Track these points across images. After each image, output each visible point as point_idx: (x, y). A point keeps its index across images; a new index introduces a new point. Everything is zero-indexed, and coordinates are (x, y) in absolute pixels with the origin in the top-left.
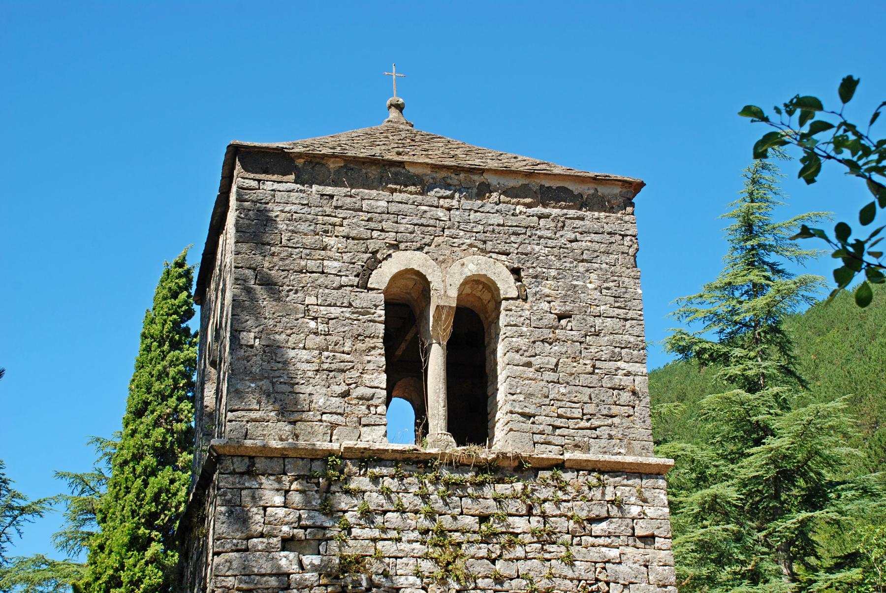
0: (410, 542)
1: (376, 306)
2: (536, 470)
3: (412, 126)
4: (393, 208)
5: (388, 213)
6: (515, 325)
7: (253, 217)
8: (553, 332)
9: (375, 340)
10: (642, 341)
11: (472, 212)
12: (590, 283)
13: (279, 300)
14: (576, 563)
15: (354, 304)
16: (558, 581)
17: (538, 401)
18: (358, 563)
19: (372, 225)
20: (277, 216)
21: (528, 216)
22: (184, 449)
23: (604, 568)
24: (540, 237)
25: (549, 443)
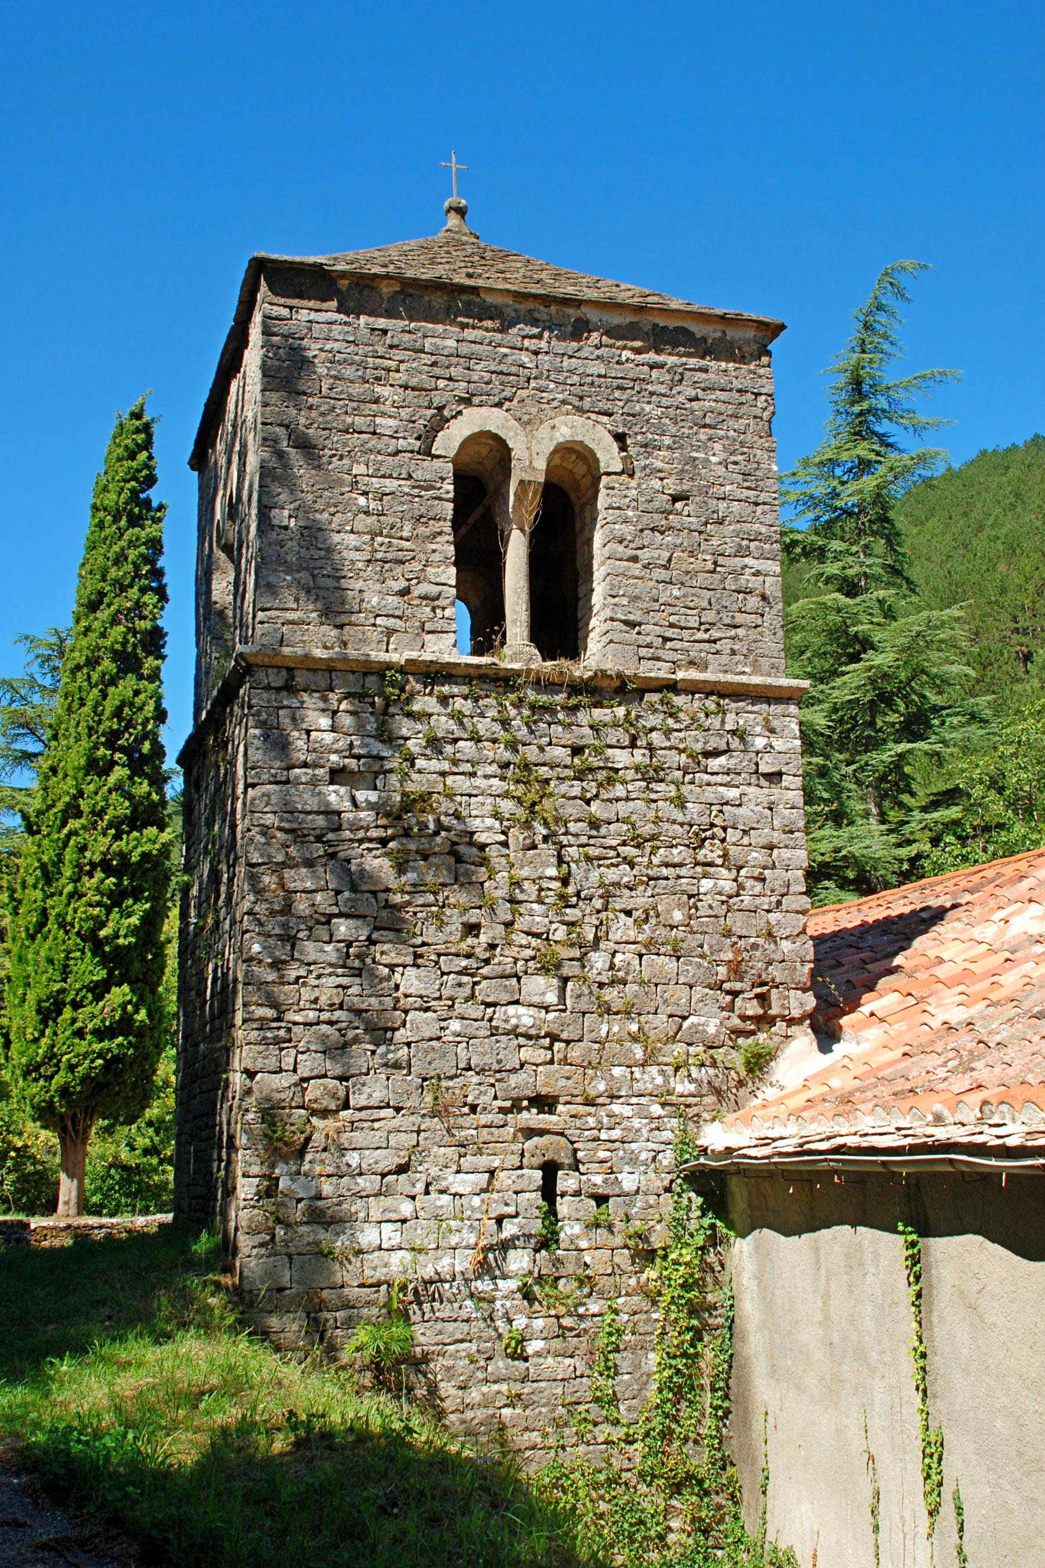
0: (487, 777)
1: (443, 479)
2: (641, 693)
3: (478, 238)
4: (465, 349)
6: (619, 508)
7: (284, 357)
13: (319, 467)
15: (414, 475)
16: (666, 826)
18: (424, 801)
19: (437, 371)
20: (315, 357)
22: (149, 653)
23: (721, 811)
24: (652, 394)
25: (658, 659)
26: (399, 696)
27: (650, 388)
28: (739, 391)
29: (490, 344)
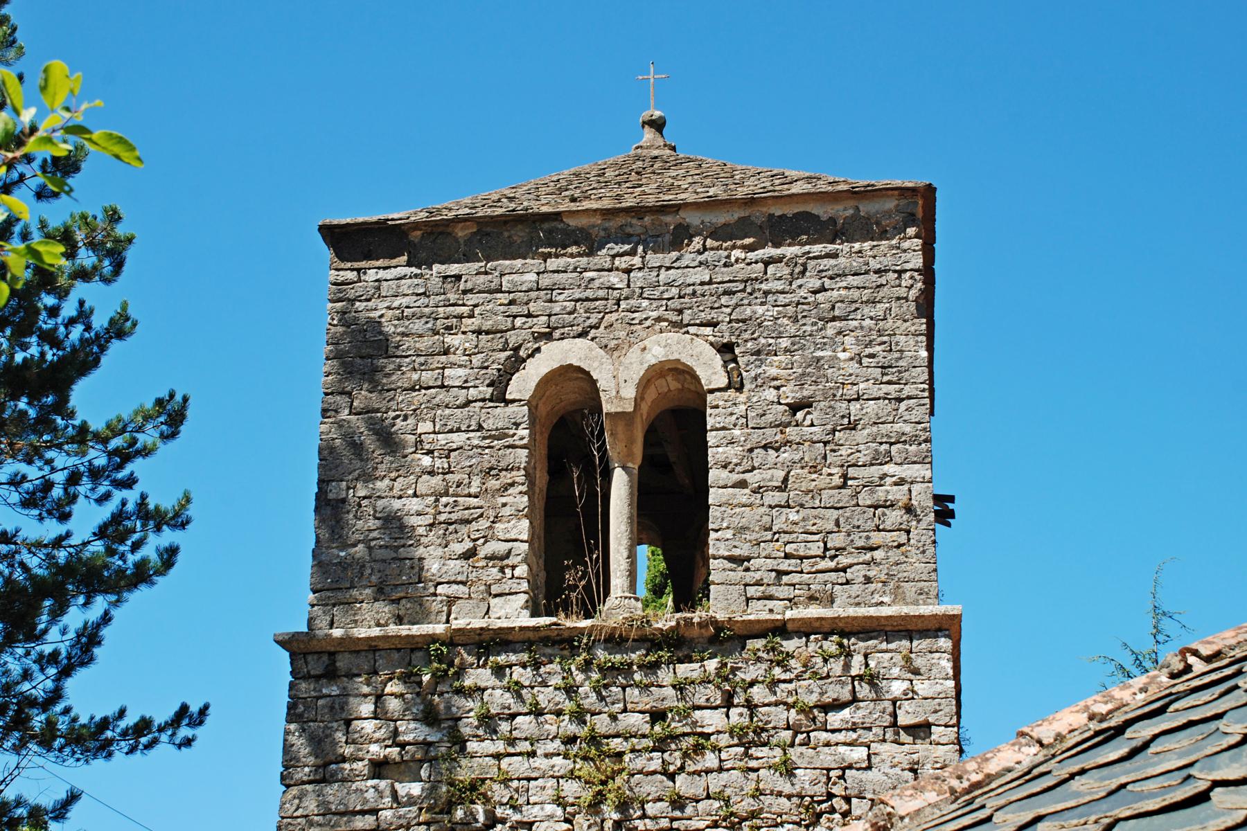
1: (517, 425)
4: (546, 281)
5: (538, 289)
6: (724, 428)
8: (782, 432)
9: (514, 473)
10: (924, 429)
12: (844, 351)
14: (797, 772)
15: (485, 425)
17: (755, 536)
19: (514, 309)
21: (749, 264)
24: (766, 293)
26: (446, 671)
27: (764, 287)
28: (877, 272)
29: (575, 270)
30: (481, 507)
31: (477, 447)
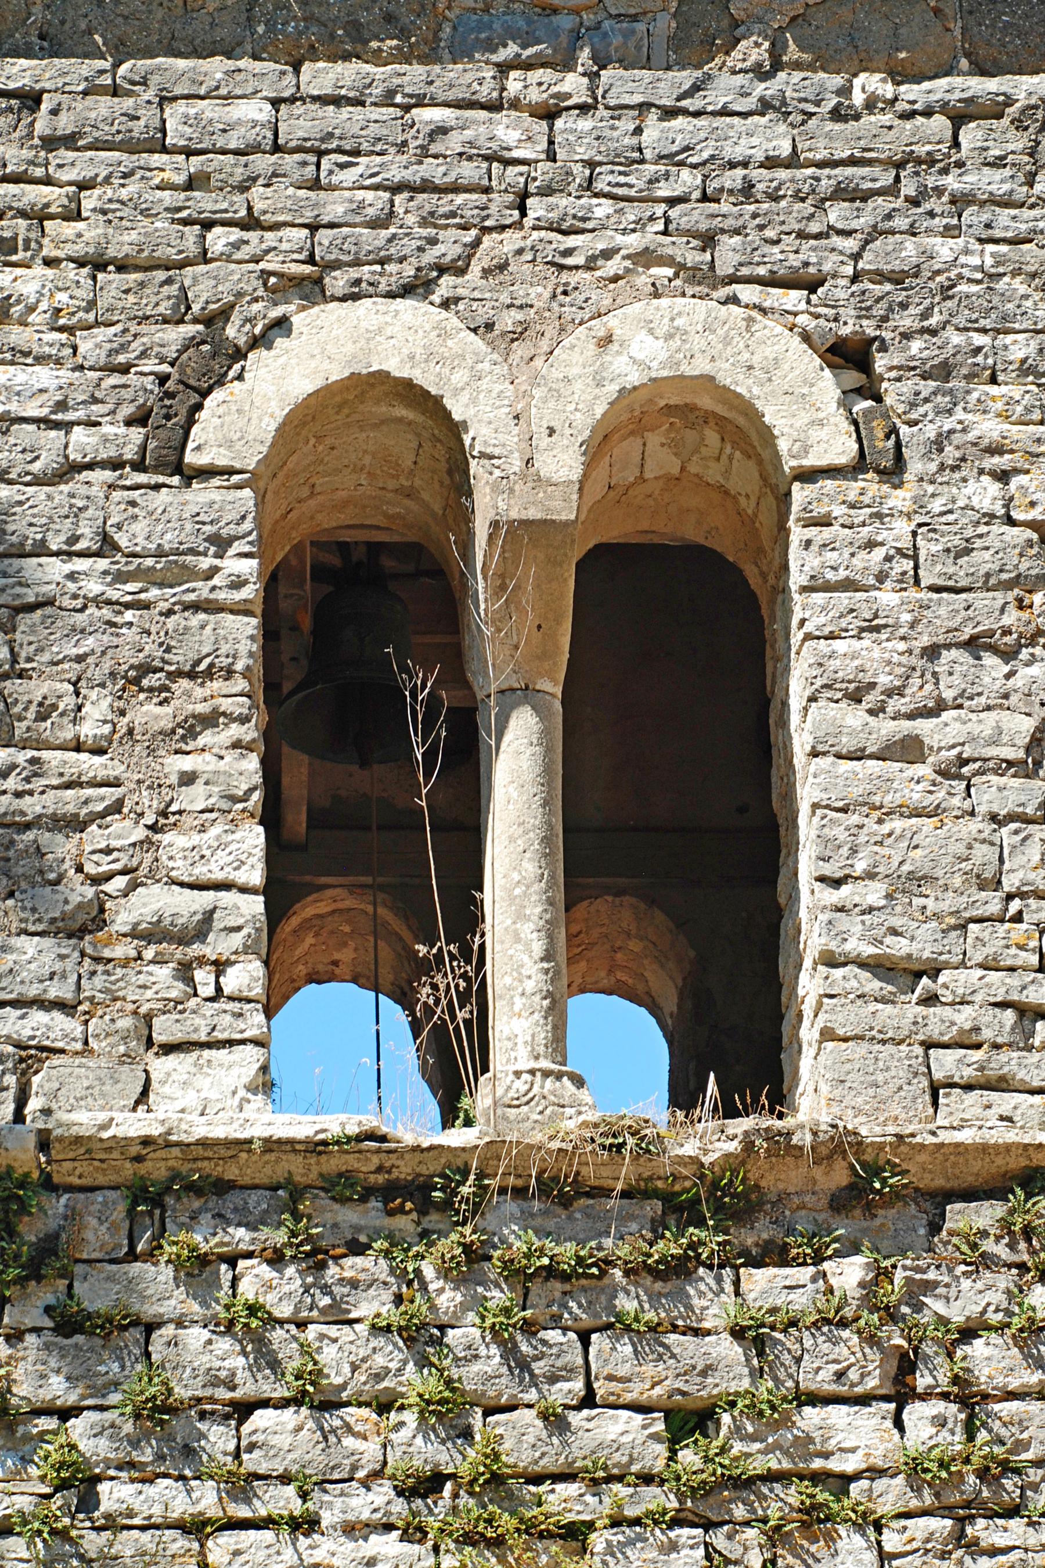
0: (352, 1530)
1: (221, 544)
4: (300, 124)
5: (277, 148)
6: (849, 585)
9: (216, 685)
11: (653, 115)
17: (949, 902)
19: (204, 202)
24: (960, 201)
25: (1001, 1084)
27: (951, 182)
29: (387, 99)
30: (116, 783)
31: (100, 601)
